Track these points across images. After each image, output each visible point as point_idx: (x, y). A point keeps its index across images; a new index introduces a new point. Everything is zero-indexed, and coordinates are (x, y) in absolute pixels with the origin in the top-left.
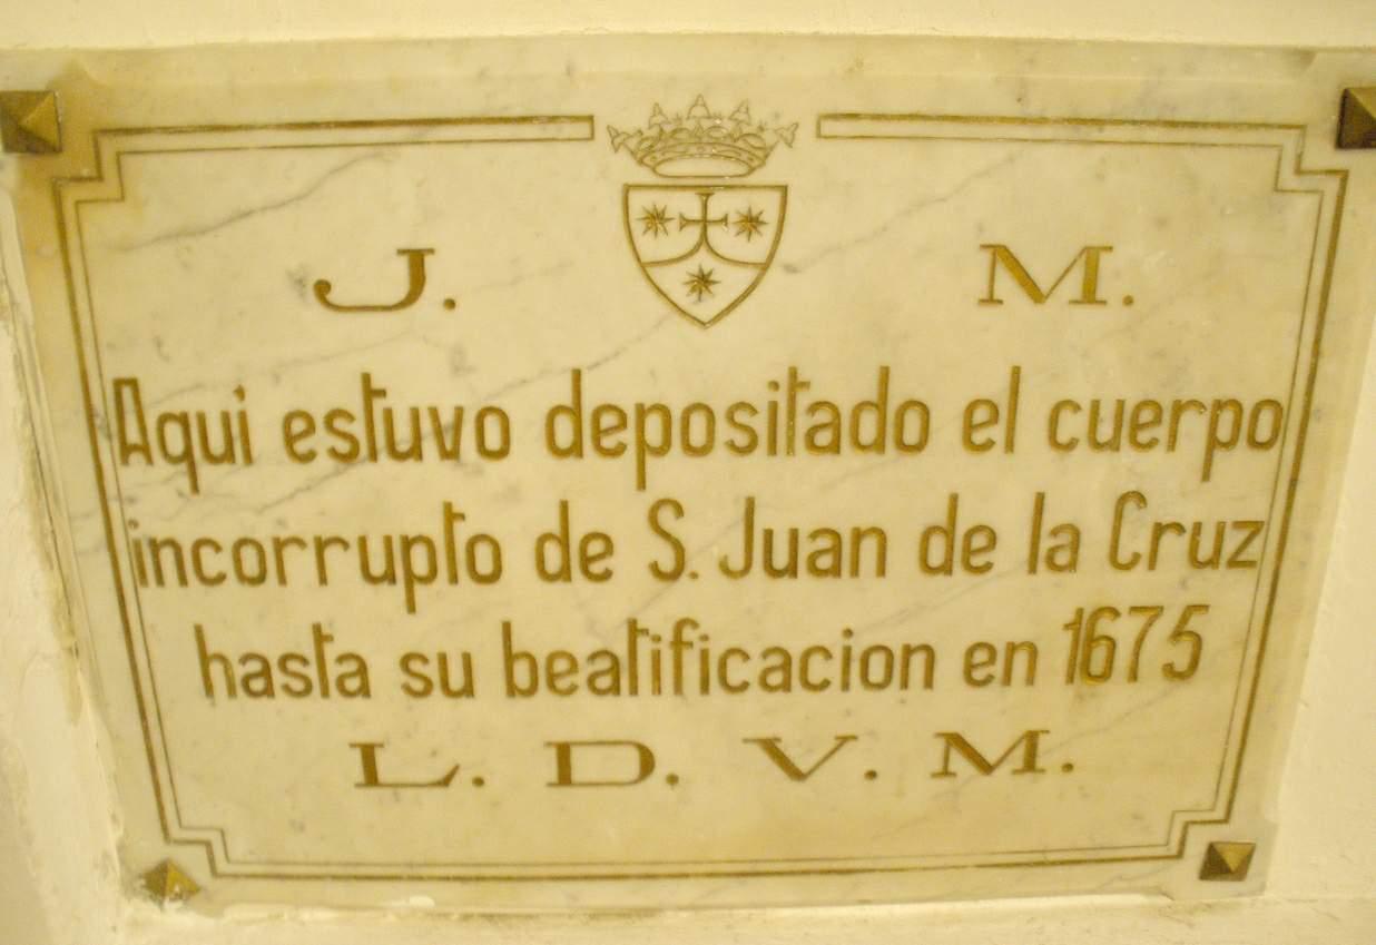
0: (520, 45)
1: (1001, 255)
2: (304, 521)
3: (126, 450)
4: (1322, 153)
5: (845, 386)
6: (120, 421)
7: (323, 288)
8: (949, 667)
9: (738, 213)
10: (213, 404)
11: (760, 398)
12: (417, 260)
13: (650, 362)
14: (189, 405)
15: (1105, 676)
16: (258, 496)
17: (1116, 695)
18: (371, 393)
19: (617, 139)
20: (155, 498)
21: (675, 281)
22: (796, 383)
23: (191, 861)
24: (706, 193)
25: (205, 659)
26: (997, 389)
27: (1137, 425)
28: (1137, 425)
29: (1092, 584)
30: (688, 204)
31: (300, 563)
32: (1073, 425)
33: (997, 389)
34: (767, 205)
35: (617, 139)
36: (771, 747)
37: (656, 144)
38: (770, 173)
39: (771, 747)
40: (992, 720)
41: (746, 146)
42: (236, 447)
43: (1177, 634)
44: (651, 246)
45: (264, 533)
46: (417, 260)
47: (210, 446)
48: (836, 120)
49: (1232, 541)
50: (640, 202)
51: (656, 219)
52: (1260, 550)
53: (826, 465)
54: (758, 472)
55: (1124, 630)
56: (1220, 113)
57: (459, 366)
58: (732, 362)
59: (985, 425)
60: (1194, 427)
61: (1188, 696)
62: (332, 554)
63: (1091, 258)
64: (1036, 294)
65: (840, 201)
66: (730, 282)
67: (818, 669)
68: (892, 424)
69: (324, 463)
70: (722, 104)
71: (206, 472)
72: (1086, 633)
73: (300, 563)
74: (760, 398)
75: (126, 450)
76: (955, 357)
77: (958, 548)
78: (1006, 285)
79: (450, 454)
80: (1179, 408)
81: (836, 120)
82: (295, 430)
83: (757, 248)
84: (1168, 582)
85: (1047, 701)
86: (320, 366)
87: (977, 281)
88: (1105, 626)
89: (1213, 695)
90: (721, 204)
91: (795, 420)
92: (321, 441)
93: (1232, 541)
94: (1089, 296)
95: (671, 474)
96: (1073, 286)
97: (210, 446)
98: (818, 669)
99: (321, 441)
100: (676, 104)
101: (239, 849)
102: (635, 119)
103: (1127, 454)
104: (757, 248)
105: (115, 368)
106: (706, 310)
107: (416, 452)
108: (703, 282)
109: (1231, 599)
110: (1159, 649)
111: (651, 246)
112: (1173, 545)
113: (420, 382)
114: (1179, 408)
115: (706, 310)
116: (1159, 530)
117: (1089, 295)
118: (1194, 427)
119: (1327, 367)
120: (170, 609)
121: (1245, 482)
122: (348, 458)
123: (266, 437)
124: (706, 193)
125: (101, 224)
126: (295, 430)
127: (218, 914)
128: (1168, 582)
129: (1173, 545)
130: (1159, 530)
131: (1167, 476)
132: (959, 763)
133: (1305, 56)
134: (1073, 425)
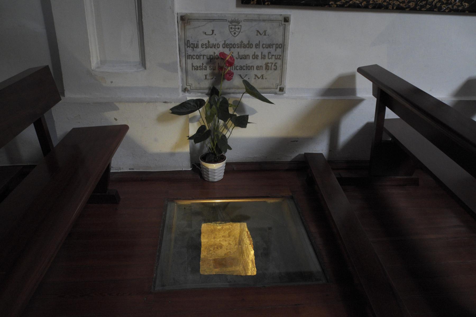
0: (221, 14)
1: (258, 31)
2: (202, 53)
3: (188, 47)
4: (283, 23)
5: (246, 42)
6: (188, 44)
7: (205, 33)
8: (255, 68)
9: (254, 112)
10: (195, 43)
11: (239, 43)
12: (213, 31)
13: (232, 40)
14: (194, 43)
15: (268, 69)
16: (199, 51)
17: (270, 72)
18: (209, 42)
19: (229, 21)
20: (190, 51)
21: (233, 33)
22: (242, 42)
23: (188, 87)
24: (235, 26)
25: (192, 66)
26: (258, 42)
27: (270, 46)
28: (270, 46)
29: (267, 60)
30: (234, 27)
31: (202, 57)
32: (264, 46)
33: (258, 42)
34: (240, 27)
35: (229, 21)
36: (240, 75)
37: (232, 22)
38: (240, 24)
39: (240, 75)
40: (259, 73)
41: (238, 22)
42: (197, 47)
43: (275, 65)
44: (231, 30)
45: (199, 54)
46: (213, 31)
47: (195, 46)
48: (245, 20)
49: (278, 57)
50: (230, 27)
51: (231, 28)
52: (281, 57)
53: (244, 49)
54: (239, 50)
55: (270, 65)
56: (275, 19)
57: (216, 40)
58: (237, 40)
59: (257, 46)
60: (274, 46)
61: (276, 71)
62: (205, 57)
63: (265, 31)
64: (261, 35)
65: (245, 26)
66: (237, 33)
67: (194, 57)
68: (249, 45)
69: (204, 48)
70: (236, 19)
71: (195, 49)
72: (267, 65)
73: (202, 57)
74: (239, 43)
75: (188, 47)
76: (255, 40)
77: (255, 57)
78: (258, 34)
79: (215, 48)
80: (273, 45)
81: (245, 20)
82: (202, 45)
83: (239, 31)
84: (273, 60)
85: (264, 72)
86: (204, 40)
87: (256, 34)
88: (268, 64)
89: (278, 72)
90: (237, 27)
91: (242, 45)
92: (204, 46)
93: (278, 57)
94: (265, 35)
95: (232, 50)
96: (264, 34)
97: (195, 46)
98: (244, 68)
99: (204, 46)
100: (233, 19)
101: (193, 86)
102: (230, 20)
103: (269, 49)
104: (239, 31)
105: (188, 39)
106: (235, 36)
107: (212, 47)
108: (235, 33)
109: (279, 62)
110: (273, 67)
111: (231, 30)
112: (273, 57)
113: (212, 42)
114: (273, 45)
115: (235, 36)
116: (272, 55)
117: (265, 35)
118: (274, 46)
119: (285, 41)
120: (190, 61)
121: (279, 51)
122: (206, 48)
123: (200, 46)
124: (235, 26)
125: (188, 27)
126: (202, 45)
127: (190, 93)
128: (273, 60)
129: (273, 57)
130: (272, 55)
131: (272, 50)
132: (256, 78)
133: (281, 15)
134: (264, 46)
